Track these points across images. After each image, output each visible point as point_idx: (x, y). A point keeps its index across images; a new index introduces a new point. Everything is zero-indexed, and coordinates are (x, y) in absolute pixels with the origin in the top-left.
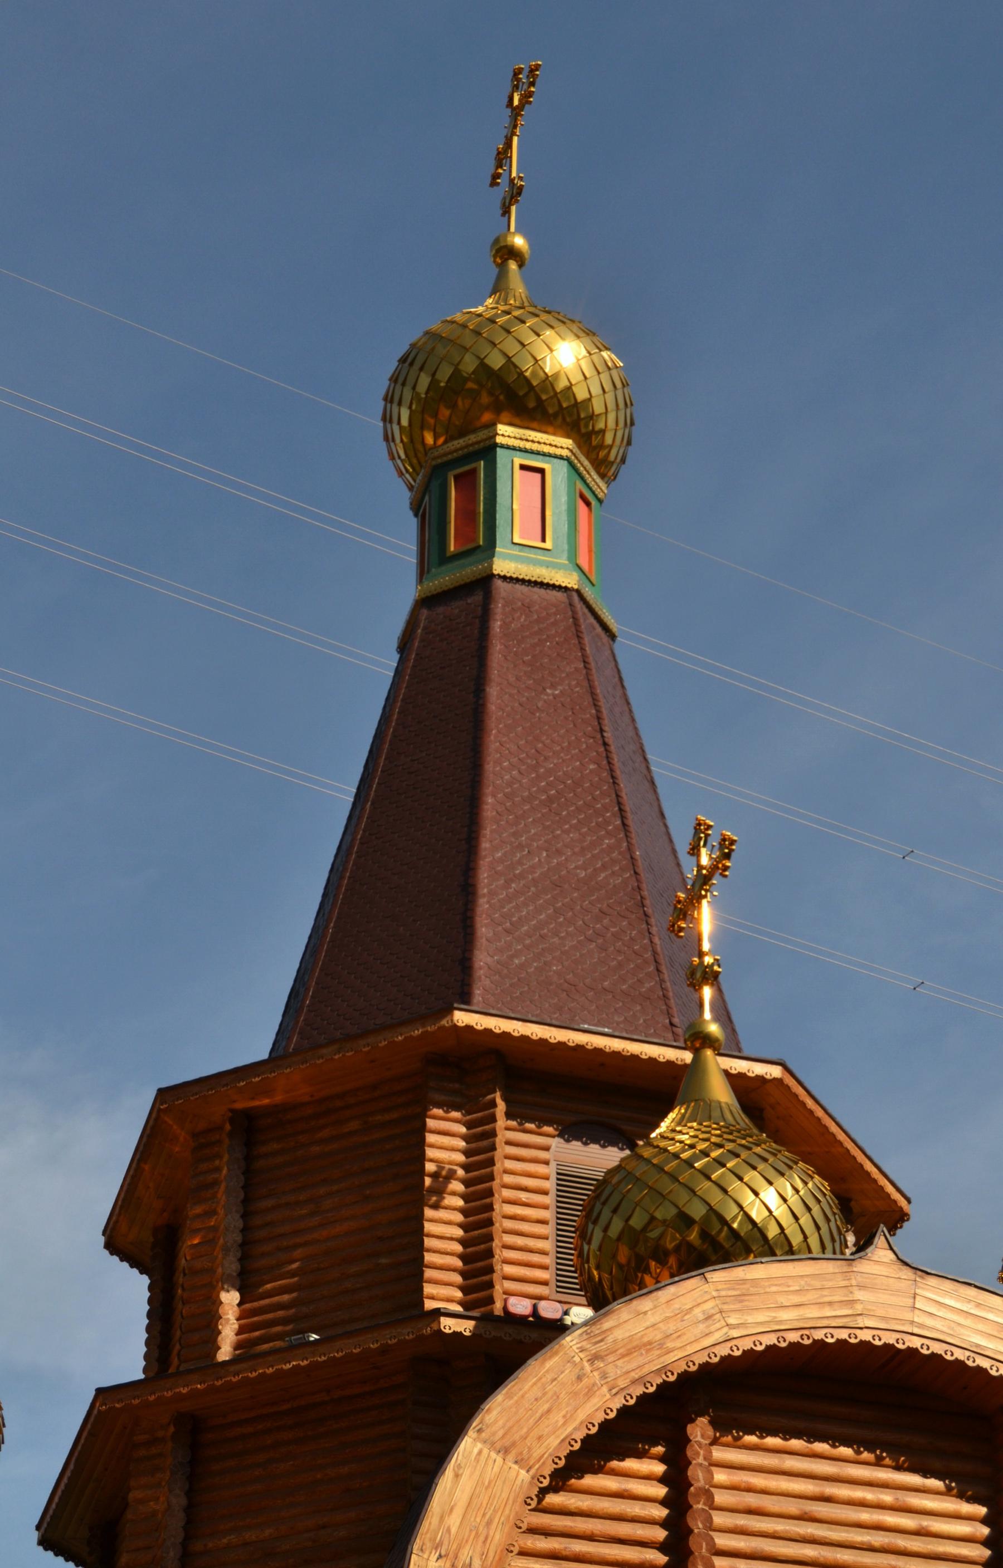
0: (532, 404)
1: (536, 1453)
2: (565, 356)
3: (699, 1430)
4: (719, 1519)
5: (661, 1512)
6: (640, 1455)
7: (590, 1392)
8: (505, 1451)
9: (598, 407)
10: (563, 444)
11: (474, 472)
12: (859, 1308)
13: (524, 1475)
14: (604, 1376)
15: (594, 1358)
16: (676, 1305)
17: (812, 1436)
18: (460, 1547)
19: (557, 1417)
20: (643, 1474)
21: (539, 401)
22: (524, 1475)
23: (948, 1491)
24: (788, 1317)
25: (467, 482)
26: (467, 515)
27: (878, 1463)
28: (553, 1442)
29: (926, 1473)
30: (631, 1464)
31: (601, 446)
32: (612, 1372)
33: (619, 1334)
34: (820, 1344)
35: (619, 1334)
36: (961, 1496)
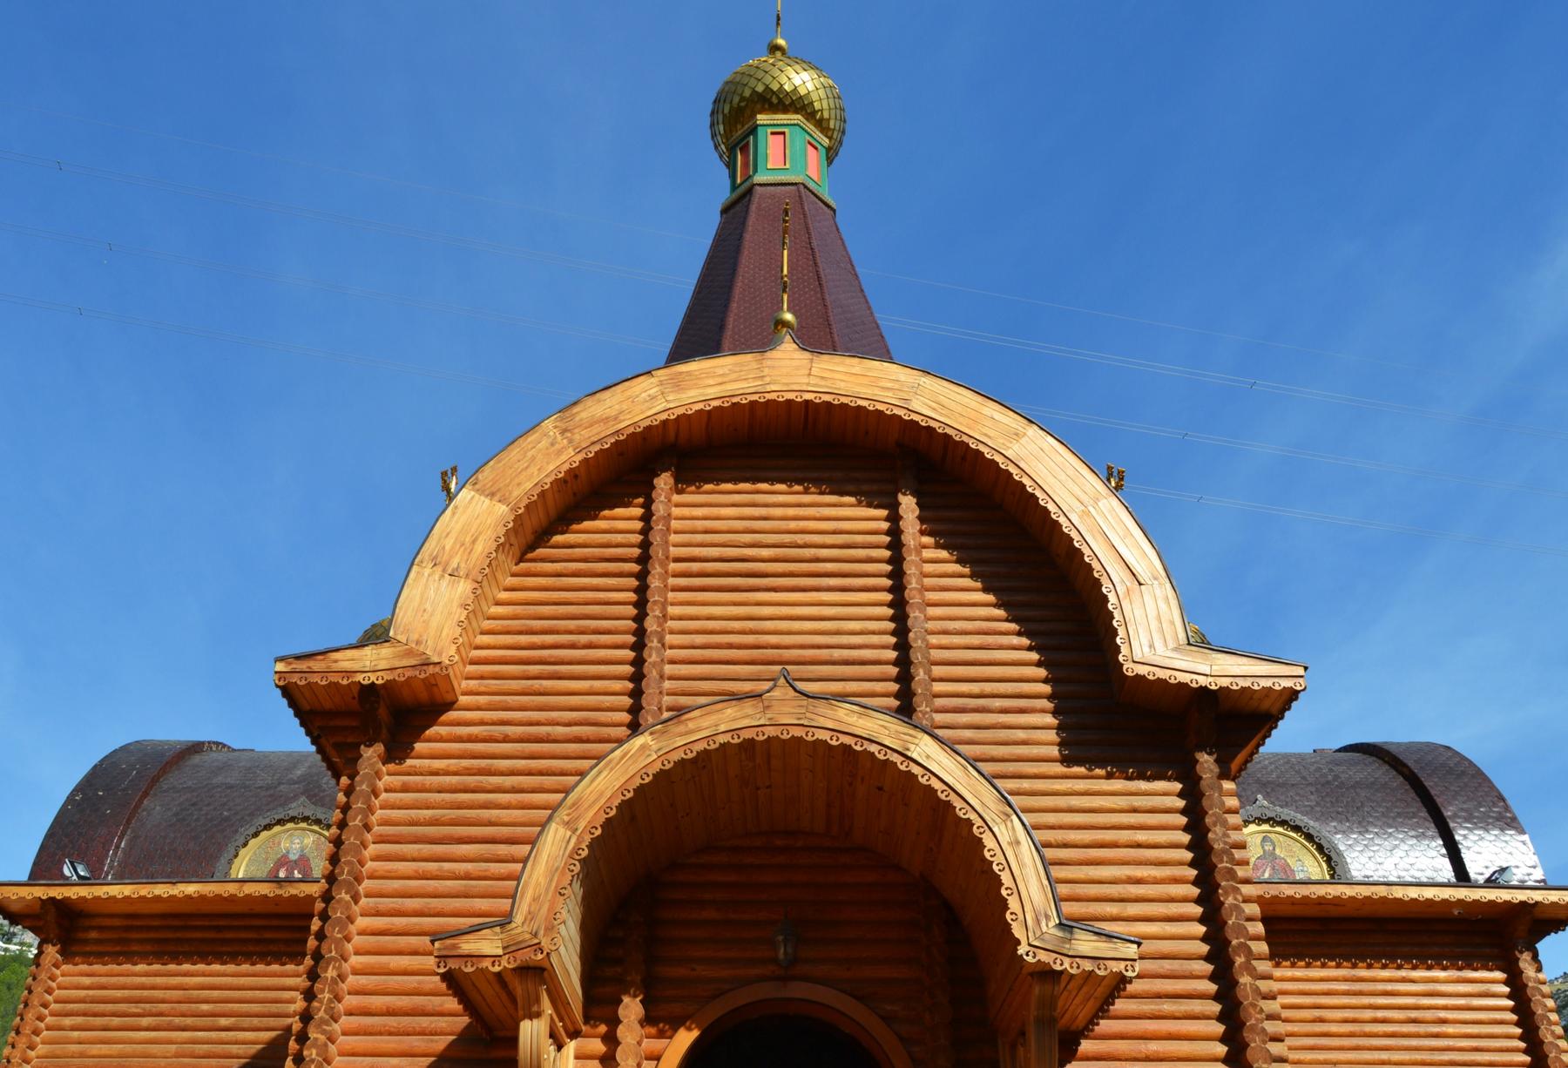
0: (775, 100)
1: (515, 494)
2: (801, 80)
3: (664, 482)
4: (673, 538)
5: (1185, 838)
6: (627, 505)
7: (559, 452)
8: (492, 495)
9: (814, 97)
10: (797, 118)
11: (747, 144)
12: (768, 379)
13: (502, 509)
14: (570, 441)
15: (564, 432)
16: (628, 393)
17: (755, 480)
18: (451, 557)
19: (534, 469)
20: (622, 521)
21: (780, 100)
22: (502, 509)
23: (859, 504)
24: (712, 392)
25: (745, 149)
26: (746, 164)
27: (806, 492)
28: (529, 485)
29: (842, 494)
30: (619, 511)
31: (822, 119)
32: (577, 437)
33: (584, 415)
34: (1115, 633)
35: (584, 415)
36: (869, 505)
